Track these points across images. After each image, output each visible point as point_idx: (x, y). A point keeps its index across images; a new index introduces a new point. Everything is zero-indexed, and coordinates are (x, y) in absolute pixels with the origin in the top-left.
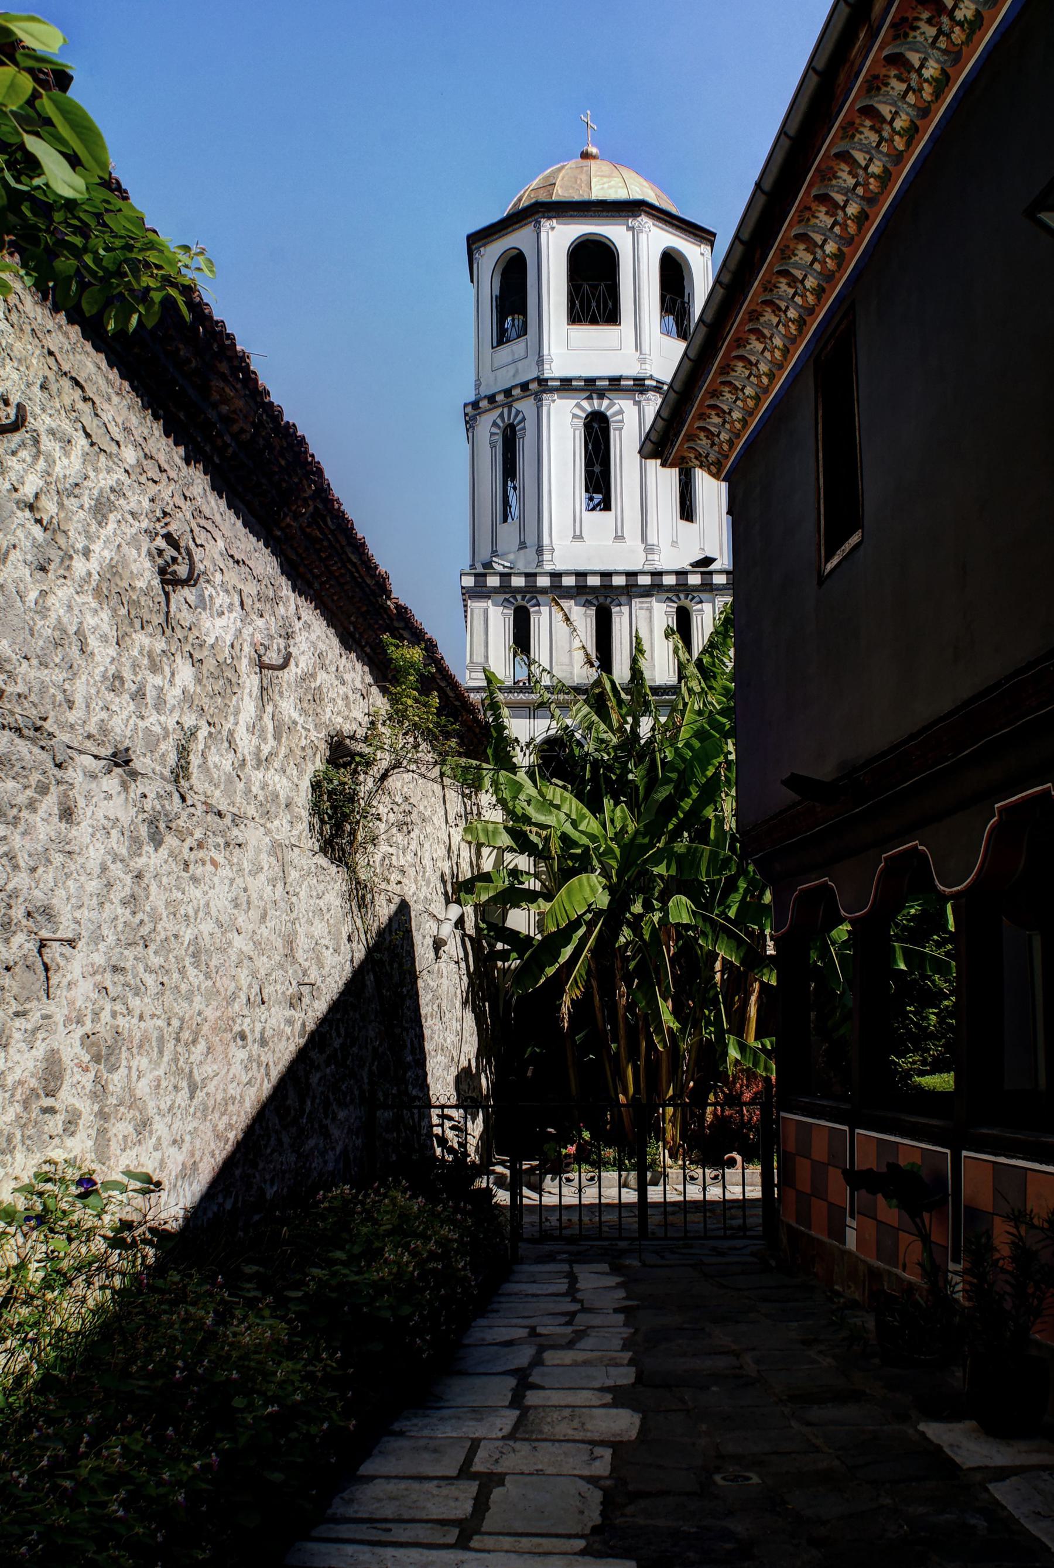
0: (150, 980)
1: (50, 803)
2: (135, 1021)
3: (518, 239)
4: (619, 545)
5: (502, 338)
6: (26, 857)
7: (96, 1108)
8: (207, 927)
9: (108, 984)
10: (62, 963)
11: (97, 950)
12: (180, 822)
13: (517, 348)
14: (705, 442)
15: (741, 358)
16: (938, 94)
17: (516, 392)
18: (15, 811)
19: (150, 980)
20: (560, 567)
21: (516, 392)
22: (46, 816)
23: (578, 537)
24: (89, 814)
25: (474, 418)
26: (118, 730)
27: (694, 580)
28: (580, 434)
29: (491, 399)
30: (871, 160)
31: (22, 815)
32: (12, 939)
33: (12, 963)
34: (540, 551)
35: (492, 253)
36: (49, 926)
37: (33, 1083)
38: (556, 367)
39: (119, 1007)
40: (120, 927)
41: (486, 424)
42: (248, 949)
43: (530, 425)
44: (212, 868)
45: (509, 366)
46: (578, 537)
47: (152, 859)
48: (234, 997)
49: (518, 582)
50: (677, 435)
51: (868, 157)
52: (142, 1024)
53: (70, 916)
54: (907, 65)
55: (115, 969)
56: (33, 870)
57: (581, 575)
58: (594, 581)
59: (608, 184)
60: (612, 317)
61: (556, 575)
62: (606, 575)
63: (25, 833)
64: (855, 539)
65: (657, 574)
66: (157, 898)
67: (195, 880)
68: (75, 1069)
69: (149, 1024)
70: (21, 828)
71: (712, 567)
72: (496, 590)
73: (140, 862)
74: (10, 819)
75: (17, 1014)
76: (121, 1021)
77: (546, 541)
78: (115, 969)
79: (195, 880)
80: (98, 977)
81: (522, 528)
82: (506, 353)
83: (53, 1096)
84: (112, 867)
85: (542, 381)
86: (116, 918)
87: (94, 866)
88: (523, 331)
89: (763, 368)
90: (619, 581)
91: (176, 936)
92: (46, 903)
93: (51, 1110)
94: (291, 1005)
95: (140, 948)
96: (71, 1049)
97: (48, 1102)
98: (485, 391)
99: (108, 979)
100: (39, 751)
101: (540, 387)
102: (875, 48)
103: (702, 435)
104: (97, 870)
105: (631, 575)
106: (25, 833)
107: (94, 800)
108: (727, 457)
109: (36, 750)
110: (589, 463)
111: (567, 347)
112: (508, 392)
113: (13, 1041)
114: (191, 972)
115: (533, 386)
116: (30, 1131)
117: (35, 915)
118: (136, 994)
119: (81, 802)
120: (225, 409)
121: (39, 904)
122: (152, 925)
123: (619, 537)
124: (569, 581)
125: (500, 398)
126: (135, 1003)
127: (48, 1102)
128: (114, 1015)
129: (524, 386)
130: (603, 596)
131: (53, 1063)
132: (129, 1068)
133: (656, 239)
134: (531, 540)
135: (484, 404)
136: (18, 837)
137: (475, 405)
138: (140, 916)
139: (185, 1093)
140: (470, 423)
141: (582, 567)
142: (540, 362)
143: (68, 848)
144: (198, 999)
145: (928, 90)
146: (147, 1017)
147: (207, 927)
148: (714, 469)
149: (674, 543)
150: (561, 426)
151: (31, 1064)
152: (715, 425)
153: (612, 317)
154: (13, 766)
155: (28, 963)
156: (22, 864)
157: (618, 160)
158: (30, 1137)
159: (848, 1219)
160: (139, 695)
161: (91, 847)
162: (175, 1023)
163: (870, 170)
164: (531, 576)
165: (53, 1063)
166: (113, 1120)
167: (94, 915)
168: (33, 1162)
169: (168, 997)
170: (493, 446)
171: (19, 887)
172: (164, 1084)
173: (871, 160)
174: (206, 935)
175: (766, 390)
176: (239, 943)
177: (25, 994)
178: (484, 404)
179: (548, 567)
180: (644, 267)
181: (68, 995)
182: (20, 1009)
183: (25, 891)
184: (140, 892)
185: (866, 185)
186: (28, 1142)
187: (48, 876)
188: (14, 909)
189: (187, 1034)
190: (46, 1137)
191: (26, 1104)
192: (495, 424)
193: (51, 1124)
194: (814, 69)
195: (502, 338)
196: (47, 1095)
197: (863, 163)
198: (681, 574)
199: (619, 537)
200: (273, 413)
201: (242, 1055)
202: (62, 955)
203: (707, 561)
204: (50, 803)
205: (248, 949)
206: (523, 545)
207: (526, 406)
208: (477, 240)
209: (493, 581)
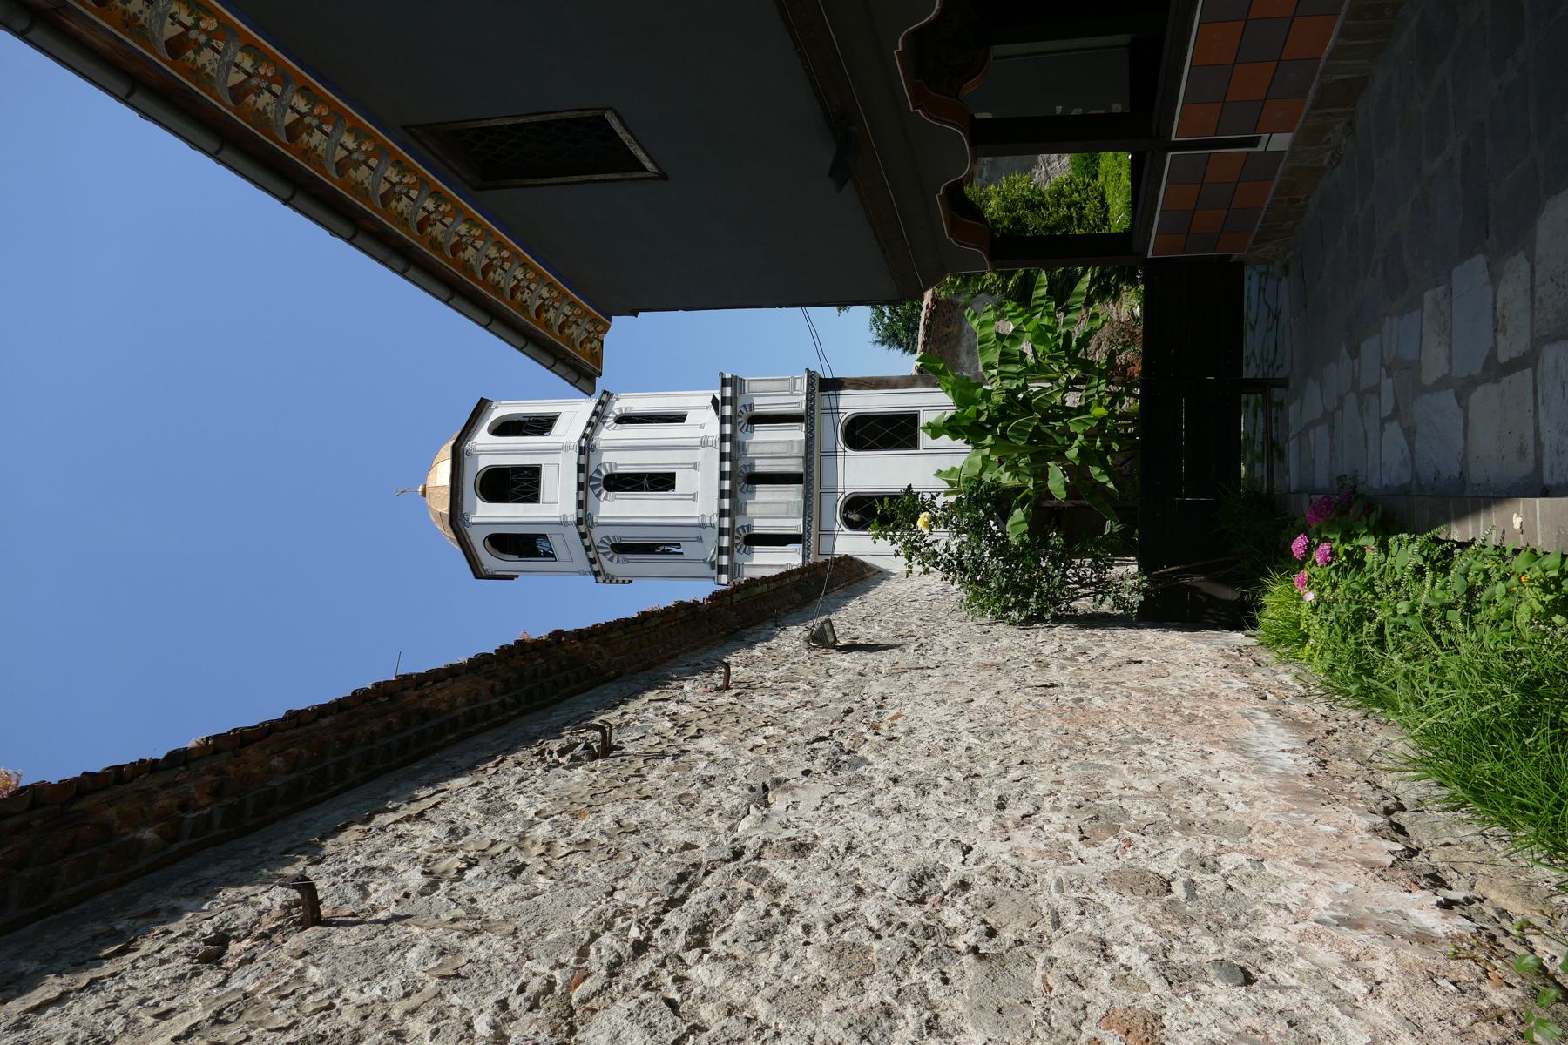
0: (1014, 774)
1: (780, 869)
2: (1064, 790)
3: (477, 539)
4: (700, 467)
5: (549, 555)
6: (839, 901)
7: (1177, 834)
8: (962, 724)
9: (1018, 814)
10: (989, 863)
11: (975, 823)
12: (846, 743)
13: (557, 544)
14: (574, 330)
15: (485, 271)
16: (478, 225)
17: (587, 542)
18: (775, 912)
19: (1014, 774)
20: (716, 510)
21: (587, 542)
22: (794, 873)
23: (694, 497)
24: (808, 826)
25: (607, 576)
26: (736, 802)
27: (728, 410)
28: (619, 494)
29: (592, 561)
30: (237, 65)
31: (783, 903)
32: (949, 925)
33: (983, 927)
34: (702, 525)
35: (490, 561)
36: (938, 876)
37: (1154, 907)
38: (570, 510)
39: (1047, 804)
40: (950, 799)
41: (611, 566)
42: (988, 694)
43: (611, 532)
44: (900, 720)
45: (568, 546)
46: (694, 497)
47: (879, 767)
48: (1038, 706)
49: (726, 542)
50: (568, 354)
51: (234, 69)
52: (1068, 782)
53: (929, 852)
54: (427, 219)
55: (1001, 806)
56: (859, 891)
57: (722, 494)
58: (727, 485)
59: (442, 474)
60: (535, 471)
61: (722, 513)
62: (723, 476)
63: (808, 901)
64: (615, 124)
65: (723, 438)
66: (920, 765)
67: (910, 732)
68: (1129, 855)
69: (1066, 773)
70: (800, 905)
71: (718, 397)
72: (731, 559)
73: (880, 781)
74: (782, 919)
75: (1057, 924)
76: (1064, 803)
77: (696, 521)
78: (1001, 806)
79: (910, 732)
80: (1010, 824)
81: (687, 540)
82: (559, 549)
83: (1168, 883)
84: (878, 804)
85: (579, 522)
86: (939, 803)
87: (871, 824)
88: (544, 536)
89: (493, 252)
90: (727, 466)
91: (968, 749)
92: (906, 878)
93: (1191, 886)
94: (1046, 666)
95: (977, 781)
96: (1099, 858)
97: (1178, 890)
98: (587, 567)
99: (1013, 812)
100: (709, 878)
101: (584, 520)
102: (82, 9)
103: (567, 331)
104: (879, 821)
105: (723, 457)
106: (808, 901)
107: (793, 819)
108: (587, 312)
109: (708, 881)
110: (640, 488)
111: (557, 501)
112: (588, 549)
113: (1096, 932)
114: (1008, 738)
115: (583, 528)
116: (1226, 915)
117: (921, 892)
118: (1032, 786)
119: (791, 833)
120: (461, 700)
121: (906, 888)
122: (953, 770)
123: (695, 466)
124: (726, 503)
125: (591, 555)
126: (1041, 789)
127: (1178, 890)
128: (1055, 809)
129: (583, 536)
130: (742, 478)
131: (1123, 880)
132: (1121, 797)
133: (483, 438)
134: (695, 532)
135: (596, 567)
136: (812, 910)
137: (597, 574)
138: (941, 780)
139: (1145, 747)
140: (610, 580)
141: (717, 494)
142: (564, 524)
143: (842, 850)
144: (1039, 733)
145: (476, 232)
146: (1059, 778)
147: (962, 724)
148: (600, 328)
149: (702, 427)
150: (616, 509)
151: (1127, 910)
152: (556, 317)
153: (535, 471)
154: (714, 911)
155: (984, 905)
156: (849, 906)
157: (428, 466)
158: (1235, 918)
159: (1260, 148)
160: (708, 782)
161: (851, 825)
162: (1065, 753)
163: (251, 70)
164: (722, 532)
165: (1123, 880)
166: (1190, 816)
167: (931, 826)
168: (1272, 916)
169: (1034, 757)
170: (627, 561)
171: (878, 911)
172: (1137, 765)
173: (237, 65)
174: (971, 725)
175: (514, 253)
176: (982, 700)
177: (1027, 911)
178: (596, 567)
179: (716, 519)
180: (501, 447)
181: (1031, 857)
182: (1048, 919)
183: (885, 904)
184: (913, 780)
185: (409, 187)
186: (1242, 919)
187: (871, 873)
188: (907, 920)
189: (1074, 744)
190: (1230, 895)
191: (1188, 921)
192: (611, 560)
193: (1210, 889)
194: (128, 96)
195: (549, 555)
196: (1169, 891)
197: (243, 77)
198: (723, 420)
199: (695, 466)
200: (480, 663)
201: (1098, 702)
202: (977, 864)
203: (714, 402)
204: (780, 869)
205: (988, 694)
206: (700, 539)
207: (597, 535)
208: (478, 572)
209: (725, 560)
